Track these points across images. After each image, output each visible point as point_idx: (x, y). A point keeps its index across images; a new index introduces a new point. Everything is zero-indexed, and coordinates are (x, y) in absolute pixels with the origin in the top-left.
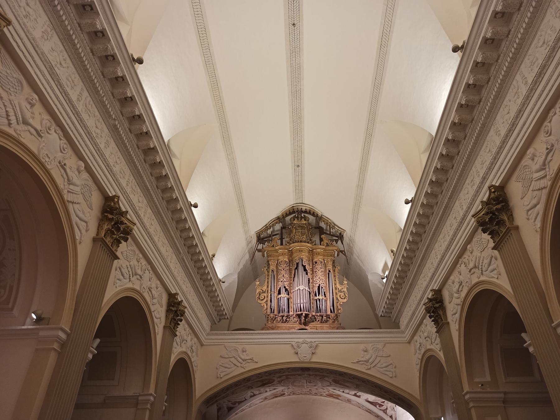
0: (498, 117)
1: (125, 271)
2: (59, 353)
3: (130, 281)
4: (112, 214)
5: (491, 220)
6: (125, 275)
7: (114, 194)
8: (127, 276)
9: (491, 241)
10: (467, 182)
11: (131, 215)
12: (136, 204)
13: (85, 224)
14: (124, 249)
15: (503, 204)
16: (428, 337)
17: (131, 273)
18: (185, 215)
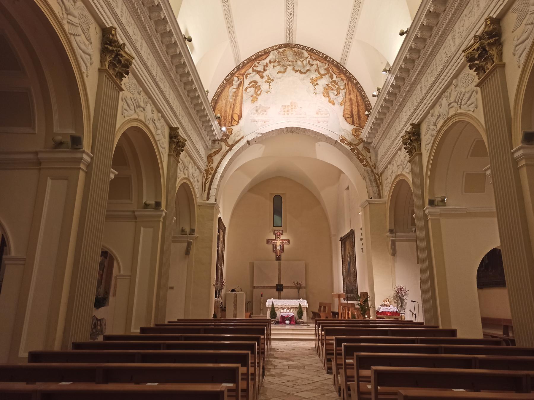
0: (456, 26)
1: (129, 102)
2: (86, 173)
3: (135, 112)
4: (111, 46)
5: (480, 56)
6: (131, 106)
7: (111, 25)
8: (132, 107)
9: (477, 77)
10: (428, 71)
11: (128, 49)
12: (133, 38)
13: (88, 57)
14: (127, 81)
15: (497, 38)
16: (401, 165)
17: (135, 104)
18: (179, 49)
